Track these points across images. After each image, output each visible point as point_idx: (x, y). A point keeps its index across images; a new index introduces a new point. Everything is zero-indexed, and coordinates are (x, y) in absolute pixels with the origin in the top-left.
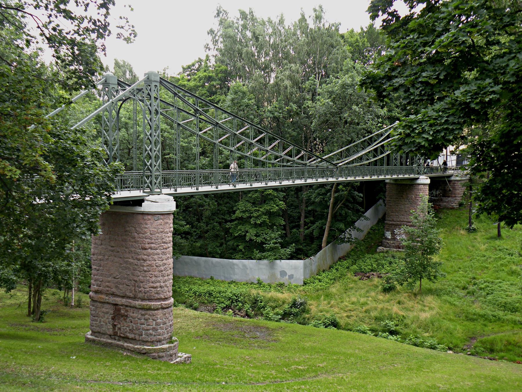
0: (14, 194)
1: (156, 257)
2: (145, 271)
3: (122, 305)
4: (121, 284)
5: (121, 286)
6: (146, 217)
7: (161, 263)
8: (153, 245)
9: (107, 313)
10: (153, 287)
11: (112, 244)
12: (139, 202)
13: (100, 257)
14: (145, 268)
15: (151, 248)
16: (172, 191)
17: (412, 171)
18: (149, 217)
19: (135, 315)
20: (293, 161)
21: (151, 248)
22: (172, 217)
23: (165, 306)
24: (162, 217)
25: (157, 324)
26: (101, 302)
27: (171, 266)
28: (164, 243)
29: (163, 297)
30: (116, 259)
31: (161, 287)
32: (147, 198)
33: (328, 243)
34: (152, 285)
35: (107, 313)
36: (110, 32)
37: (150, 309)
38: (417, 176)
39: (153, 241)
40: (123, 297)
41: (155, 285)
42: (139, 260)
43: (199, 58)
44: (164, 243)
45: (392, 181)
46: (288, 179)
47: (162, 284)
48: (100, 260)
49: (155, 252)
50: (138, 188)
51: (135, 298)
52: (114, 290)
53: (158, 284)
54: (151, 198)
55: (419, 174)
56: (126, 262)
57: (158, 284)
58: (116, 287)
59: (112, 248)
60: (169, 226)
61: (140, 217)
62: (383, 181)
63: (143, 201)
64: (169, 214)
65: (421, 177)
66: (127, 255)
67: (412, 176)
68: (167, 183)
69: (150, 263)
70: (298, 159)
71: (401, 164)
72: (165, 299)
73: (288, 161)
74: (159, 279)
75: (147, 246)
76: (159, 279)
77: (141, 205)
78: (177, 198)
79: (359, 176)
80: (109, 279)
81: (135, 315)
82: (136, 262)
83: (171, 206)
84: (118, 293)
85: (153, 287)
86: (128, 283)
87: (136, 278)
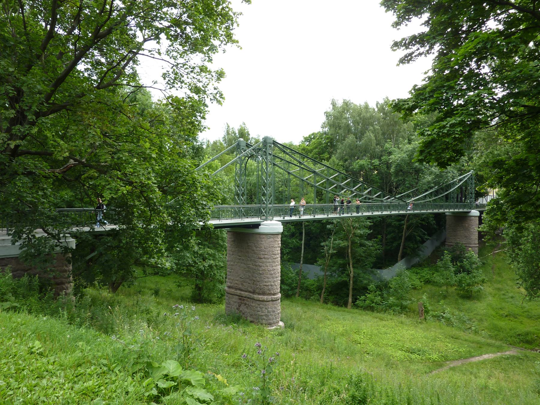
0: (152, 227)
1: (268, 264)
2: (261, 274)
3: (245, 297)
4: (244, 282)
5: (245, 284)
6: (262, 236)
7: (271, 269)
8: (266, 256)
9: (235, 302)
10: (266, 286)
11: (239, 254)
12: (257, 225)
13: (232, 263)
14: (261, 272)
15: (264, 258)
16: (281, 219)
17: (464, 207)
18: (264, 236)
19: (253, 304)
20: (373, 198)
21: (264, 258)
22: (280, 236)
23: (274, 299)
24: (272, 236)
25: (269, 312)
26: (231, 294)
27: (280, 270)
28: (273, 254)
29: (272, 292)
30: (242, 265)
31: (271, 285)
32: (262, 223)
33: (402, 257)
34: (265, 284)
35: (235, 302)
36: (421, 17)
37: (263, 301)
38: (469, 210)
39: (266, 253)
40: (246, 291)
41: (267, 284)
42: (256, 266)
43: (366, 103)
44: (273, 254)
45: (450, 214)
46: (378, 211)
47: (272, 284)
48: (232, 265)
49: (268, 261)
50: (258, 216)
51: (254, 292)
52: (240, 286)
53: (269, 283)
54: (265, 222)
55: (470, 209)
56: (249, 267)
57: (269, 283)
58: (242, 284)
59: (239, 258)
60: (278, 243)
61: (258, 236)
62: (444, 213)
63: (260, 225)
64: (277, 234)
65: (472, 211)
66: (249, 263)
67: (465, 210)
68: (278, 212)
69: (264, 268)
70: (376, 197)
71: (457, 201)
72: (274, 294)
73: (369, 199)
74: (270, 280)
75: (262, 256)
76: (270, 280)
77: (258, 228)
78: (285, 223)
79: (430, 209)
80: (238, 279)
81: (253, 304)
82: (254, 267)
83: (280, 228)
84: (243, 289)
85: (266, 286)
86: (249, 282)
87: (254, 279)
